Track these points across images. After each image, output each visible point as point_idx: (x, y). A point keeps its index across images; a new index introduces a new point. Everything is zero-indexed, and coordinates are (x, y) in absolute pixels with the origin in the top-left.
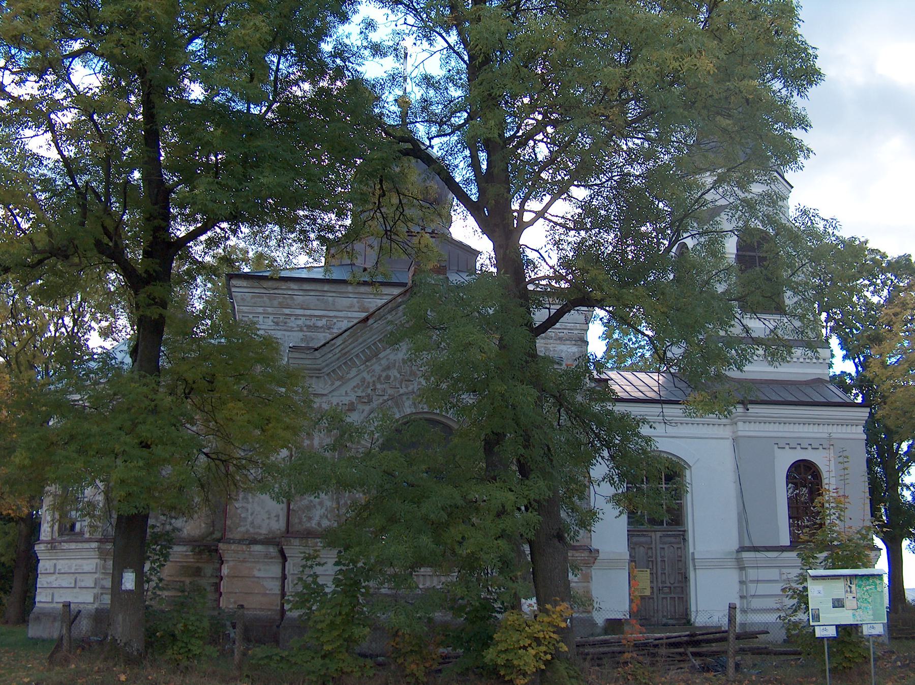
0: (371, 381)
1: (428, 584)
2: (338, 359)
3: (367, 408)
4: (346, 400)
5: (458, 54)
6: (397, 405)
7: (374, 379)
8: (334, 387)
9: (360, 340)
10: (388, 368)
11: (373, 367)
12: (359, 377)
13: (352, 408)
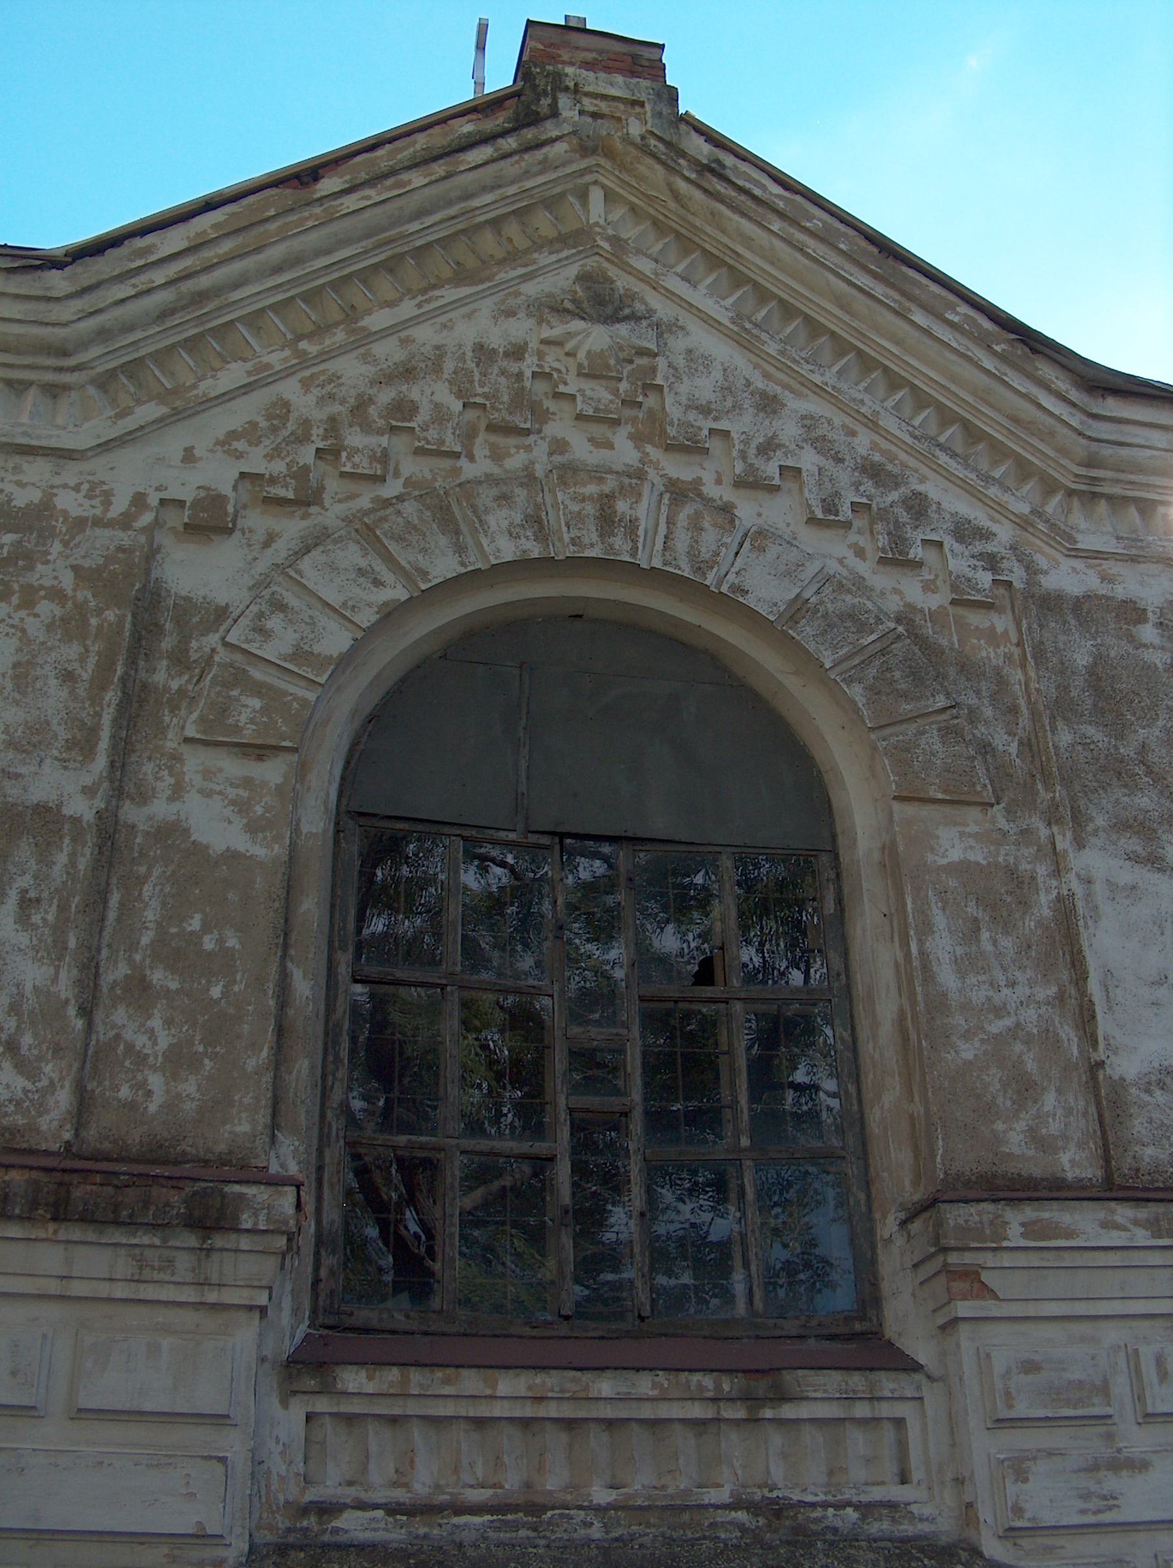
0: (319, 415)
1: (641, 1482)
2: (165, 314)
3: (292, 528)
4: (185, 486)
5: (150, 1246)
6: (449, 524)
7: (336, 408)
8: (129, 423)
9: (276, 253)
10: (407, 372)
11: (332, 366)
12: (262, 397)
13: (208, 522)
